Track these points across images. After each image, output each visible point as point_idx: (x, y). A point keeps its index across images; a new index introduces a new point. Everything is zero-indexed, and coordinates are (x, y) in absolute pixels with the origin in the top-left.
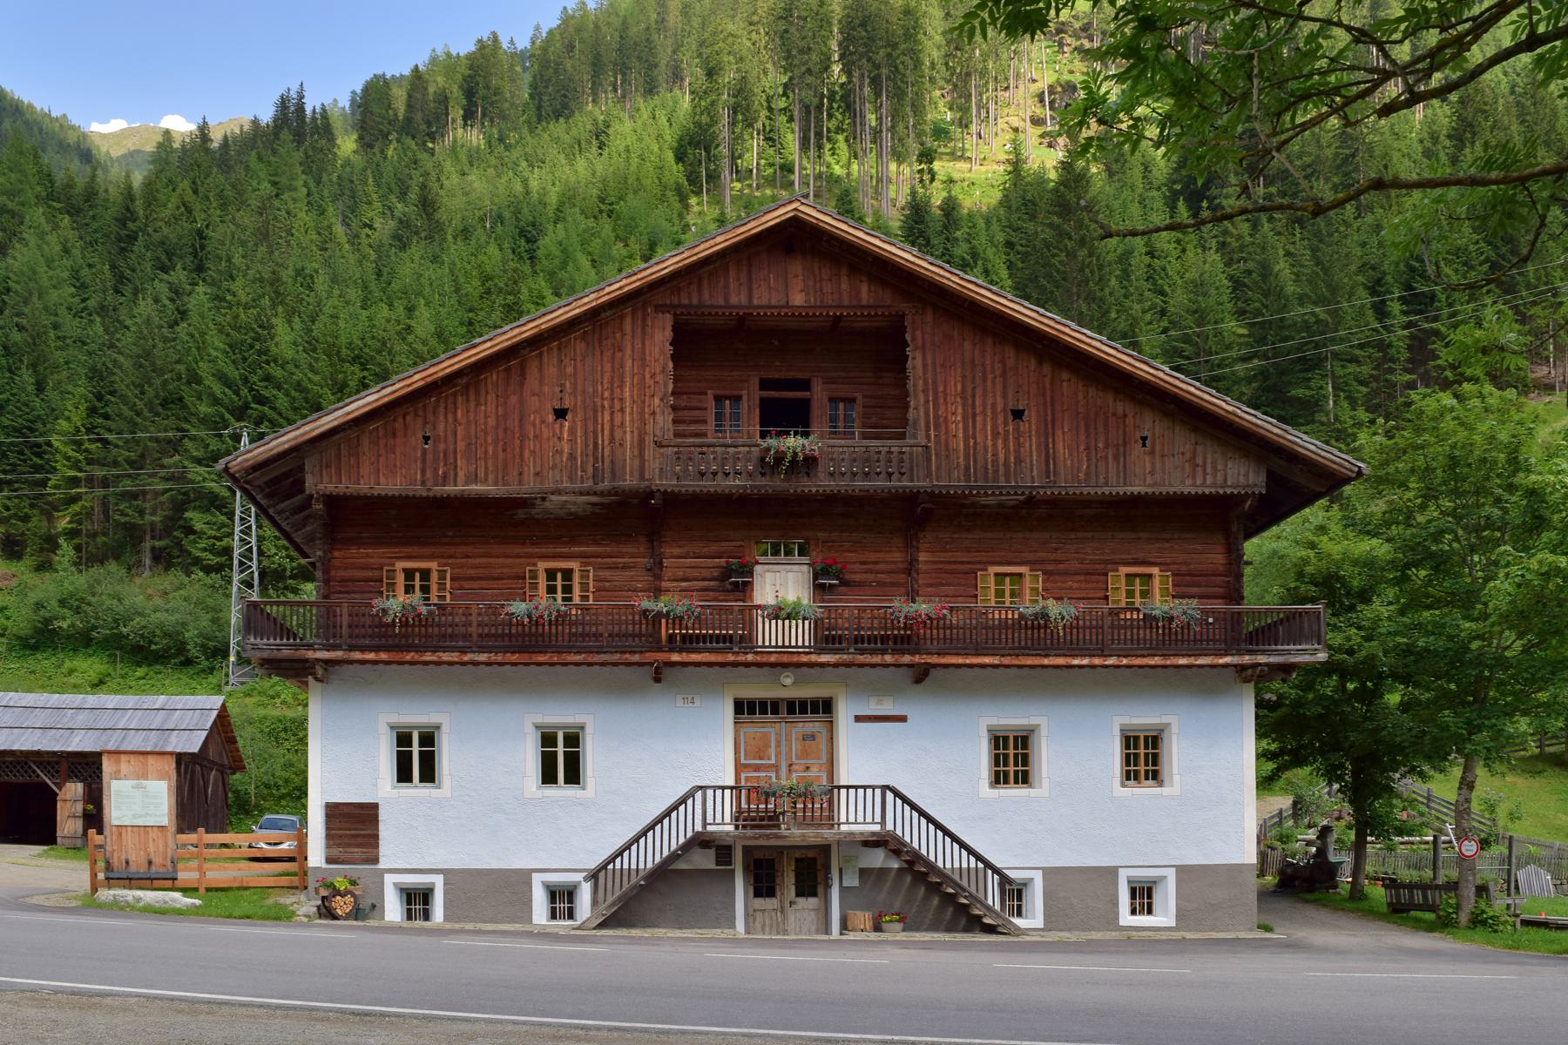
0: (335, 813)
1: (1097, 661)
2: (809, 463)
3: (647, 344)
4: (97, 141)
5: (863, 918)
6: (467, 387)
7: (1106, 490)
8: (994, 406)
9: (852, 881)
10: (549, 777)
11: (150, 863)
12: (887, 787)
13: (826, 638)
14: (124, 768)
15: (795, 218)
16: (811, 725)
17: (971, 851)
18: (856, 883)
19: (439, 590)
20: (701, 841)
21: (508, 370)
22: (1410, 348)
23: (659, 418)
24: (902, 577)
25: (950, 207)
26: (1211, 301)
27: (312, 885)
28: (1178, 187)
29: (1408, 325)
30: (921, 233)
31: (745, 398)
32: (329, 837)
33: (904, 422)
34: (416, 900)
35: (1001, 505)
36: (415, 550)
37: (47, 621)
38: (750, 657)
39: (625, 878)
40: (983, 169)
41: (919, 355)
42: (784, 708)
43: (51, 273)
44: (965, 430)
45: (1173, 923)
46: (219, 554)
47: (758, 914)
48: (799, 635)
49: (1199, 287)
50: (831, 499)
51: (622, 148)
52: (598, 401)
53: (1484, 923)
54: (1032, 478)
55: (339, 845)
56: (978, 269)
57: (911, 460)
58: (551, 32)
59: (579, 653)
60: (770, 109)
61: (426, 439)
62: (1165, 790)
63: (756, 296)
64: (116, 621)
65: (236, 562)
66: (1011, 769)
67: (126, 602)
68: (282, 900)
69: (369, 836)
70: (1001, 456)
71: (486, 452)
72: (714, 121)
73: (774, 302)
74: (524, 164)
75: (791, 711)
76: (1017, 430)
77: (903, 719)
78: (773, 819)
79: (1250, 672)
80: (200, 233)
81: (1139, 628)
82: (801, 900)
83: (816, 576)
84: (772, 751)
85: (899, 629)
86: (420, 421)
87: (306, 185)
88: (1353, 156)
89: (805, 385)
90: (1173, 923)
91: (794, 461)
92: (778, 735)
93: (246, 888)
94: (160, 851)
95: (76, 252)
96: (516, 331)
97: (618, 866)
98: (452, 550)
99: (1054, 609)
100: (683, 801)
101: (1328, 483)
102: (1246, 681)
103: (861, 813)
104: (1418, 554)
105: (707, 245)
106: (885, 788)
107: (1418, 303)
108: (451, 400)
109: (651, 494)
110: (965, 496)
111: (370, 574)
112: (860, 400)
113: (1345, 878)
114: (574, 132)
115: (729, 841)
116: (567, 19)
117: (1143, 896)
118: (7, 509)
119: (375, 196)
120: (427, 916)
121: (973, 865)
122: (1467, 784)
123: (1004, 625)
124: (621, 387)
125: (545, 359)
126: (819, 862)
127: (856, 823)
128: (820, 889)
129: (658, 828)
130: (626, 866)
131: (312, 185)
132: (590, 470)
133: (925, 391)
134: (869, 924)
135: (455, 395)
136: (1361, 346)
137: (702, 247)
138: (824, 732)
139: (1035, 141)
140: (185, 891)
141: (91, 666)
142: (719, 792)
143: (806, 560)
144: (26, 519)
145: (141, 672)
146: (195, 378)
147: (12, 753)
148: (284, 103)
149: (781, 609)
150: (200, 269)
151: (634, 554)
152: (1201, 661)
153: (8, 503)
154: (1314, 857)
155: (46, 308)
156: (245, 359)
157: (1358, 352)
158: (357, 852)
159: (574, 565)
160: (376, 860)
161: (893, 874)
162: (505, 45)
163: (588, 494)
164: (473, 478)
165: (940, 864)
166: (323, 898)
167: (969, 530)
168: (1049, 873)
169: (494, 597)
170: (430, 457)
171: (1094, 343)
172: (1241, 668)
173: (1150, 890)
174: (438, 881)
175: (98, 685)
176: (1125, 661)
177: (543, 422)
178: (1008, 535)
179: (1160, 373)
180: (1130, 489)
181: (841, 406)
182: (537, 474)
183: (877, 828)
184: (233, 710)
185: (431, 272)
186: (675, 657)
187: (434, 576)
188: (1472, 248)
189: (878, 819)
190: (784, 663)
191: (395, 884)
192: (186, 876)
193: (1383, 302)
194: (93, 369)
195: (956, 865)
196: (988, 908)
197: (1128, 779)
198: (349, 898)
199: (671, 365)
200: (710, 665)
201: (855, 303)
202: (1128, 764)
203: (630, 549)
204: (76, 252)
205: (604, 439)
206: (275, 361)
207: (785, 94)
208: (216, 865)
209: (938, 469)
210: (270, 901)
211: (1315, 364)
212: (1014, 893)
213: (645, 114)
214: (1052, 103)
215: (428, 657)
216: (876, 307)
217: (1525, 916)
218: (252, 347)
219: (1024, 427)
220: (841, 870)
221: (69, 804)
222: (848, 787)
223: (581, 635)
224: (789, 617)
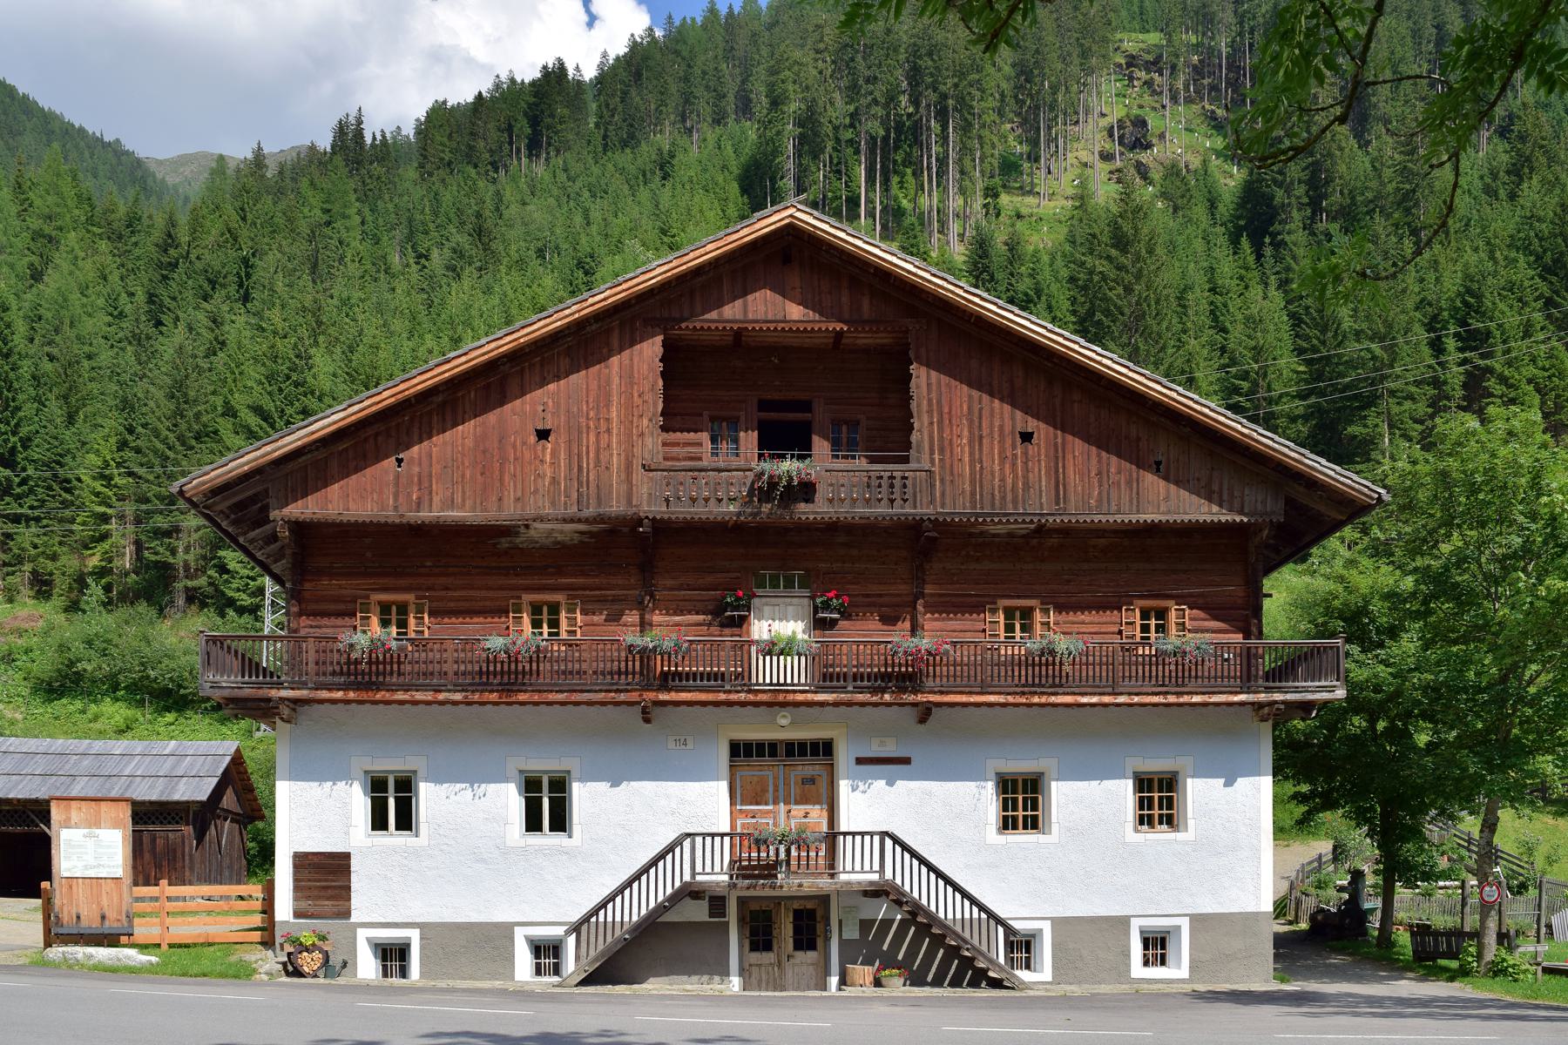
1: (1106, 699)
2: (806, 490)
4: (153, 167)
8: (1001, 427)
9: (852, 933)
10: (533, 824)
11: (103, 917)
12: (886, 833)
13: (827, 678)
14: (75, 816)
16: (808, 767)
17: (974, 902)
18: (856, 935)
19: (417, 625)
20: (690, 892)
21: (487, 387)
22: (1465, 386)
23: (649, 441)
25: (1013, 246)
27: (278, 940)
28: (1242, 223)
29: (1464, 362)
30: (986, 269)
31: (743, 419)
32: (297, 889)
33: (908, 446)
34: (393, 956)
35: (1011, 535)
37: (72, 664)
38: (742, 696)
40: (1052, 204)
42: (781, 750)
43: (85, 300)
44: (971, 454)
46: (253, 595)
48: (792, 671)
51: (686, 179)
52: (583, 420)
53: (1504, 972)
54: (1039, 504)
56: (1042, 306)
57: (914, 485)
58: (617, 59)
59: (562, 691)
60: (838, 140)
62: (1180, 836)
64: (142, 664)
65: (267, 602)
67: (156, 645)
68: (247, 957)
70: (1009, 481)
71: (463, 476)
72: (776, 152)
74: (587, 194)
76: (1025, 454)
77: (906, 761)
78: (768, 870)
79: (1266, 710)
80: (245, 261)
82: (800, 955)
85: (900, 665)
87: (359, 212)
88: (1414, 191)
89: (806, 406)
91: (789, 486)
93: (210, 944)
94: (114, 907)
95: (114, 278)
96: (493, 345)
97: (601, 919)
100: (670, 849)
101: (1352, 509)
102: (1263, 720)
103: (708, 862)
104: (1440, 584)
106: (884, 834)
107: (1473, 340)
109: (640, 522)
113: (1375, 922)
114: (640, 161)
115: (719, 892)
116: (634, 46)
117: (1157, 946)
118: (35, 547)
119: (432, 226)
120: (404, 973)
121: (976, 915)
122: (1490, 826)
124: (608, 406)
125: (527, 375)
126: (819, 915)
127: (853, 871)
128: (820, 942)
129: (644, 878)
130: (610, 919)
131: (366, 211)
133: (930, 412)
134: (869, 979)
136: (1418, 383)
137: (692, 255)
138: (825, 775)
139: (1104, 176)
140: (143, 947)
141: (114, 711)
142: (708, 839)
144: (54, 557)
145: (170, 717)
146: (230, 412)
147: (8, 801)
148: (341, 129)
149: (774, 644)
150: (246, 298)
153: (36, 540)
154: (1346, 903)
155: (78, 337)
156: (281, 390)
157: (1413, 389)
158: (328, 905)
160: (347, 914)
162: (571, 72)
163: (572, 521)
164: (451, 504)
165: (941, 915)
166: (289, 954)
167: (977, 560)
170: (403, 480)
171: (1105, 361)
172: (1258, 706)
173: (1163, 940)
174: (414, 936)
175: (123, 731)
177: (524, 443)
179: (1209, 409)
180: (1142, 517)
181: (844, 428)
183: (875, 877)
184: (246, 754)
185: (480, 301)
186: (663, 697)
188: (1527, 283)
189: (876, 867)
190: (778, 701)
191: (368, 939)
192: (144, 930)
193: (1439, 338)
194: (125, 400)
195: (959, 916)
196: (991, 961)
197: (1141, 823)
198: (317, 955)
199: (661, 383)
200: (704, 704)
202: (1141, 808)
204: (114, 278)
206: (312, 393)
208: (180, 919)
209: (943, 494)
210: (233, 959)
211: (1371, 401)
212: (1022, 946)
213: (711, 143)
214: (1121, 138)
215: (400, 696)
217: (1545, 964)
218: (288, 378)
219: (1032, 449)
220: (840, 922)
223: (564, 672)
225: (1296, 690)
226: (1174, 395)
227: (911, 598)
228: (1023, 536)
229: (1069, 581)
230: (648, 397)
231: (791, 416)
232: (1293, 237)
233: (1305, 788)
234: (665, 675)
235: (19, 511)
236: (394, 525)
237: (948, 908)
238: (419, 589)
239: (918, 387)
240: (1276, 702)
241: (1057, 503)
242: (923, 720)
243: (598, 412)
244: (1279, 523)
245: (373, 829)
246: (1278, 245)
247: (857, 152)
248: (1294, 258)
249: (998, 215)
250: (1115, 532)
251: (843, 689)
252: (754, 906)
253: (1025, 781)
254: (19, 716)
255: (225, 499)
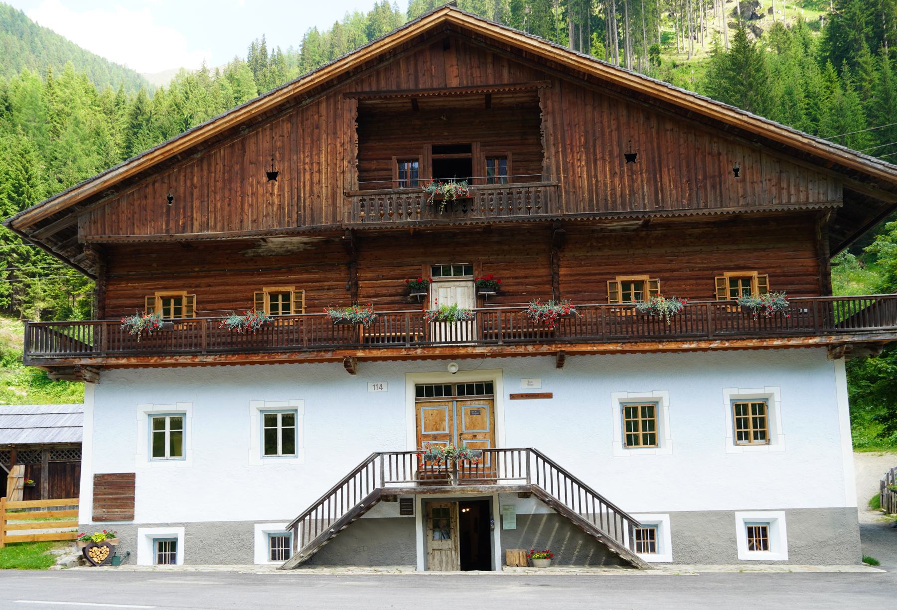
0: (101, 481)
3: (338, 122)
5: (516, 555)
6: (201, 160)
7: (706, 211)
8: (611, 153)
9: (511, 525)
12: (531, 449)
13: (486, 337)
15: (446, 22)
17: (602, 500)
18: (513, 526)
20: (381, 496)
21: (232, 146)
24: (547, 287)
26: (849, 120)
32: (95, 500)
33: (540, 169)
34: (166, 549)
36: (170, 282)
39: (319, 524)
41: (549, 118)
42: (455, 390)
43: (84, 147)
44: (588, 172)
45: (786, 558)
47: (436, 553)
48: (465, 333)
49: (839, 111)
50: (488, 230)
52: (301, 166)
55: (103, 507)
57: (545, 197)
61: (170, 199)
63: (421, 81)
66: (641, 433)
69: (127, 498)
70: (619, 190)
71: (215, 207)
73: (435, 86)
75: (461, 392)
77: (549, 396)
78: (442, 478)
79: (838, 349)
81: (738, 318)
83: (477, 291)
84: (446, 424)
86: (165, 186)
89: (468, 148)
90: (786, 558)
92: (451, 411)
93: (33, 543)
98: (198, 281)
99: (663, 304)
100: (365, 465)
102: (837, 357)
105: (378, 45)
108: (189, 170)
110: (594, 222)
111: (135, 301)
112: (509, 154)
117: (758, 535)
120: (173, 559)
123: (630, 321)
124: (319, 154)
130: (319, 517)
132: (295, 216)
135: (193, 165)
137: (374, 47)
138: (487, 408)
143: (470, 277)
151: (337, 278)
152: (793, 342)
153: (45, 288)
159: (291, 289)
160: (131, 517)
161: (544, 519)
166: (84, 549)
167: (599, 249)
168: (675, 516)
169: (217, 314)
172: (831, 347)
173: (764, 529)
176: (727, 344)
177: (258, 183)
178: (631, 252)
181: (496, 162)
182: (254, 221)
183: (523, 483)
187: (184, 301)
189: (524, 475)
191: (264, 532)
195: (591, 511)
198: (105, 549)
199: (356, 136)
201: (498, 82)
203: (334, 275)
205: (305, 193)
207: (563, 19)
209: (567, 202)
212: (646, 536)
215: (168, 360)
216: (514, 84)
220: (501, 516)
221: (15, 480)
222: (505, 450)
224: (445, 320)
225: (863, 333)
226: (745, 118)
227: (550, 278)
228: (634, 230)
229: (672, 261)
230: (348, 146)
231: (456, 156)
232: (864, 59)
233: (884, 412)
234: (366, 340)
235: (35, 270)
236: (165, 243)
237: (581, 506)
238: (190, 287)
239: (546, 128)
240: (846, 343)
241: (657, 203)
242: (560, 365)
243: (311, 159)
244: (838, 207)
245: (154, 455)
246: (853, 65)
247: (567, 35)
248: (865, 71)
249: (659, 64)
250: (707, 224)
251: (495, 344)
252: (436, 506)
253: (643, 408)
254: (25, 394)
255: (46, 230)
